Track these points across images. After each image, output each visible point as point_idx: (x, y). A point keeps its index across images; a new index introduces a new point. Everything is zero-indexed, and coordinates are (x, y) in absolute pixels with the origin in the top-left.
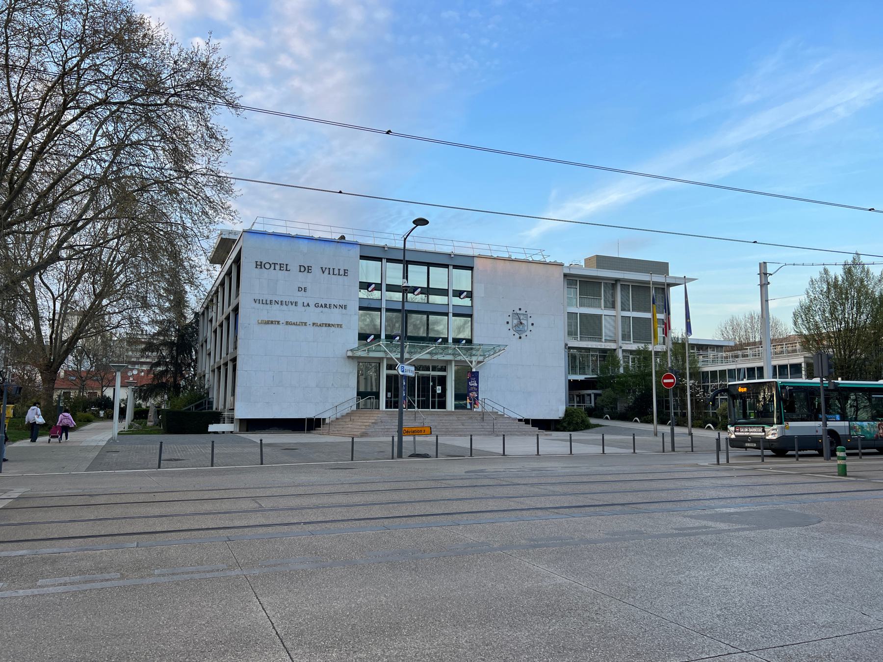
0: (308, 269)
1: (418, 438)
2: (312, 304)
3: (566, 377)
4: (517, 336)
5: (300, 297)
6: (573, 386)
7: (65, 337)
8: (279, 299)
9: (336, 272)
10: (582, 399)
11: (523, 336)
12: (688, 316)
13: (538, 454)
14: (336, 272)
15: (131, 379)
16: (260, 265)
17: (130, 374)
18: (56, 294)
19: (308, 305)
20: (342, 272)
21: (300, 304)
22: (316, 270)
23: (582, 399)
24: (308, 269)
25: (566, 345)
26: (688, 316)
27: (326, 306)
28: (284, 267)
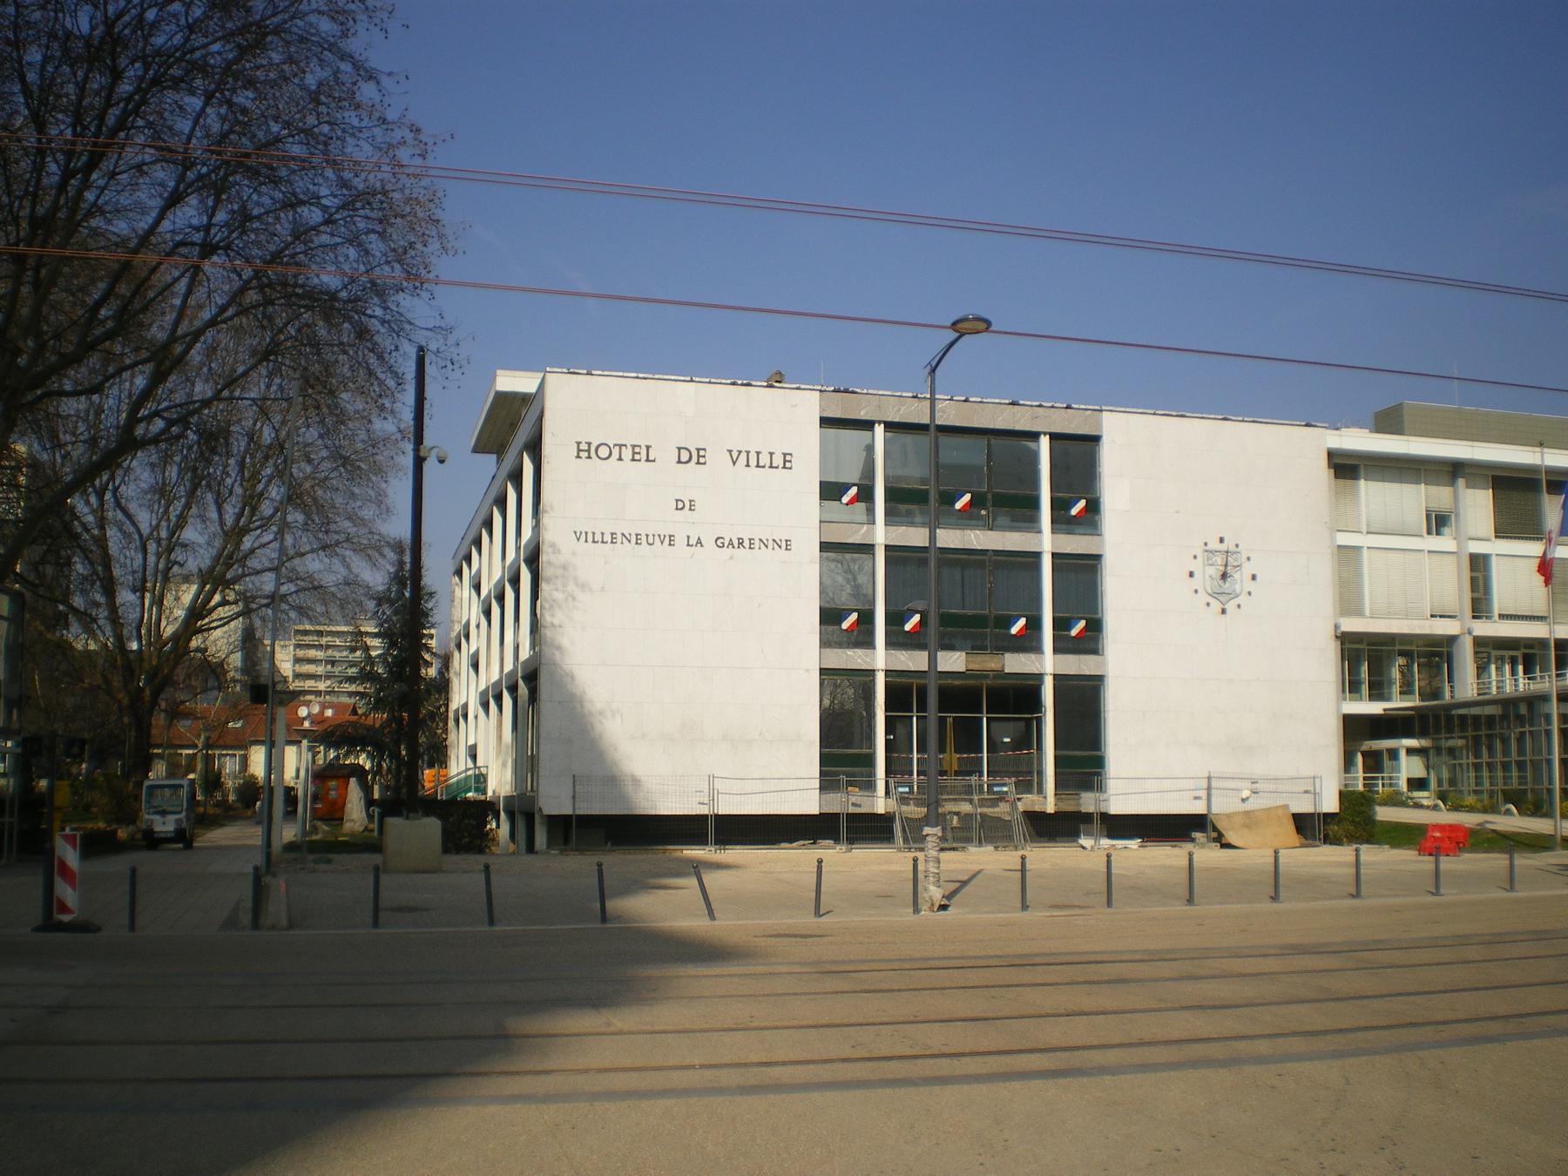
0: (699, 456)
1: (1447, 863)
2: (709, 541)
3: (1338, 708)
4: (1216, 606)
5: (682, 525)
6: (1355, 729)
7: (168, 630)
8: (631, 530)
9: (765, 460)
10: (1374, 762)
11: (1230, 607)
12: (475, 285)
13: (49, 925)
14: (765, 460)
15: (307, 724)
16: (585, 451)
17: (303, 712)
18: (146, 531)
19: (699, 542)
20: (778, 460)
21: (680, 541)
22: (717, 458)
23: (1374, 762)
24: (699, 456)
25: (1336, 627)
26: (475, 285)
27: (741, 543)
28: (641, 454)
